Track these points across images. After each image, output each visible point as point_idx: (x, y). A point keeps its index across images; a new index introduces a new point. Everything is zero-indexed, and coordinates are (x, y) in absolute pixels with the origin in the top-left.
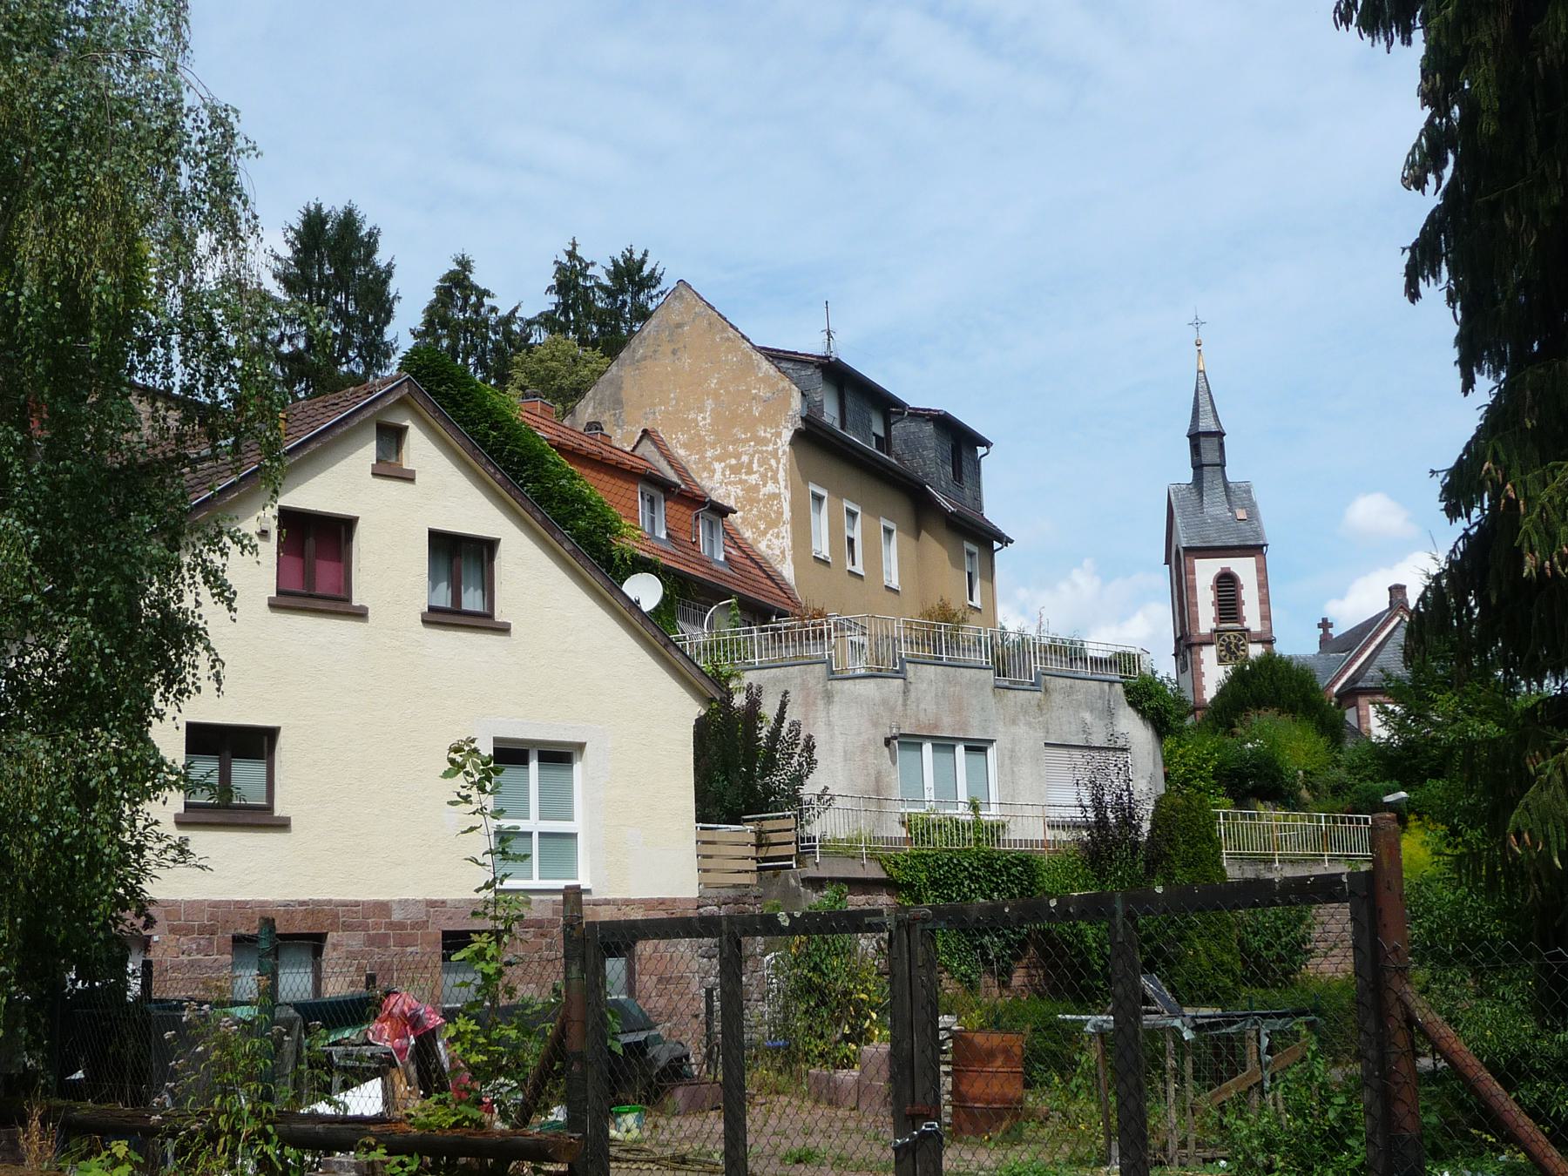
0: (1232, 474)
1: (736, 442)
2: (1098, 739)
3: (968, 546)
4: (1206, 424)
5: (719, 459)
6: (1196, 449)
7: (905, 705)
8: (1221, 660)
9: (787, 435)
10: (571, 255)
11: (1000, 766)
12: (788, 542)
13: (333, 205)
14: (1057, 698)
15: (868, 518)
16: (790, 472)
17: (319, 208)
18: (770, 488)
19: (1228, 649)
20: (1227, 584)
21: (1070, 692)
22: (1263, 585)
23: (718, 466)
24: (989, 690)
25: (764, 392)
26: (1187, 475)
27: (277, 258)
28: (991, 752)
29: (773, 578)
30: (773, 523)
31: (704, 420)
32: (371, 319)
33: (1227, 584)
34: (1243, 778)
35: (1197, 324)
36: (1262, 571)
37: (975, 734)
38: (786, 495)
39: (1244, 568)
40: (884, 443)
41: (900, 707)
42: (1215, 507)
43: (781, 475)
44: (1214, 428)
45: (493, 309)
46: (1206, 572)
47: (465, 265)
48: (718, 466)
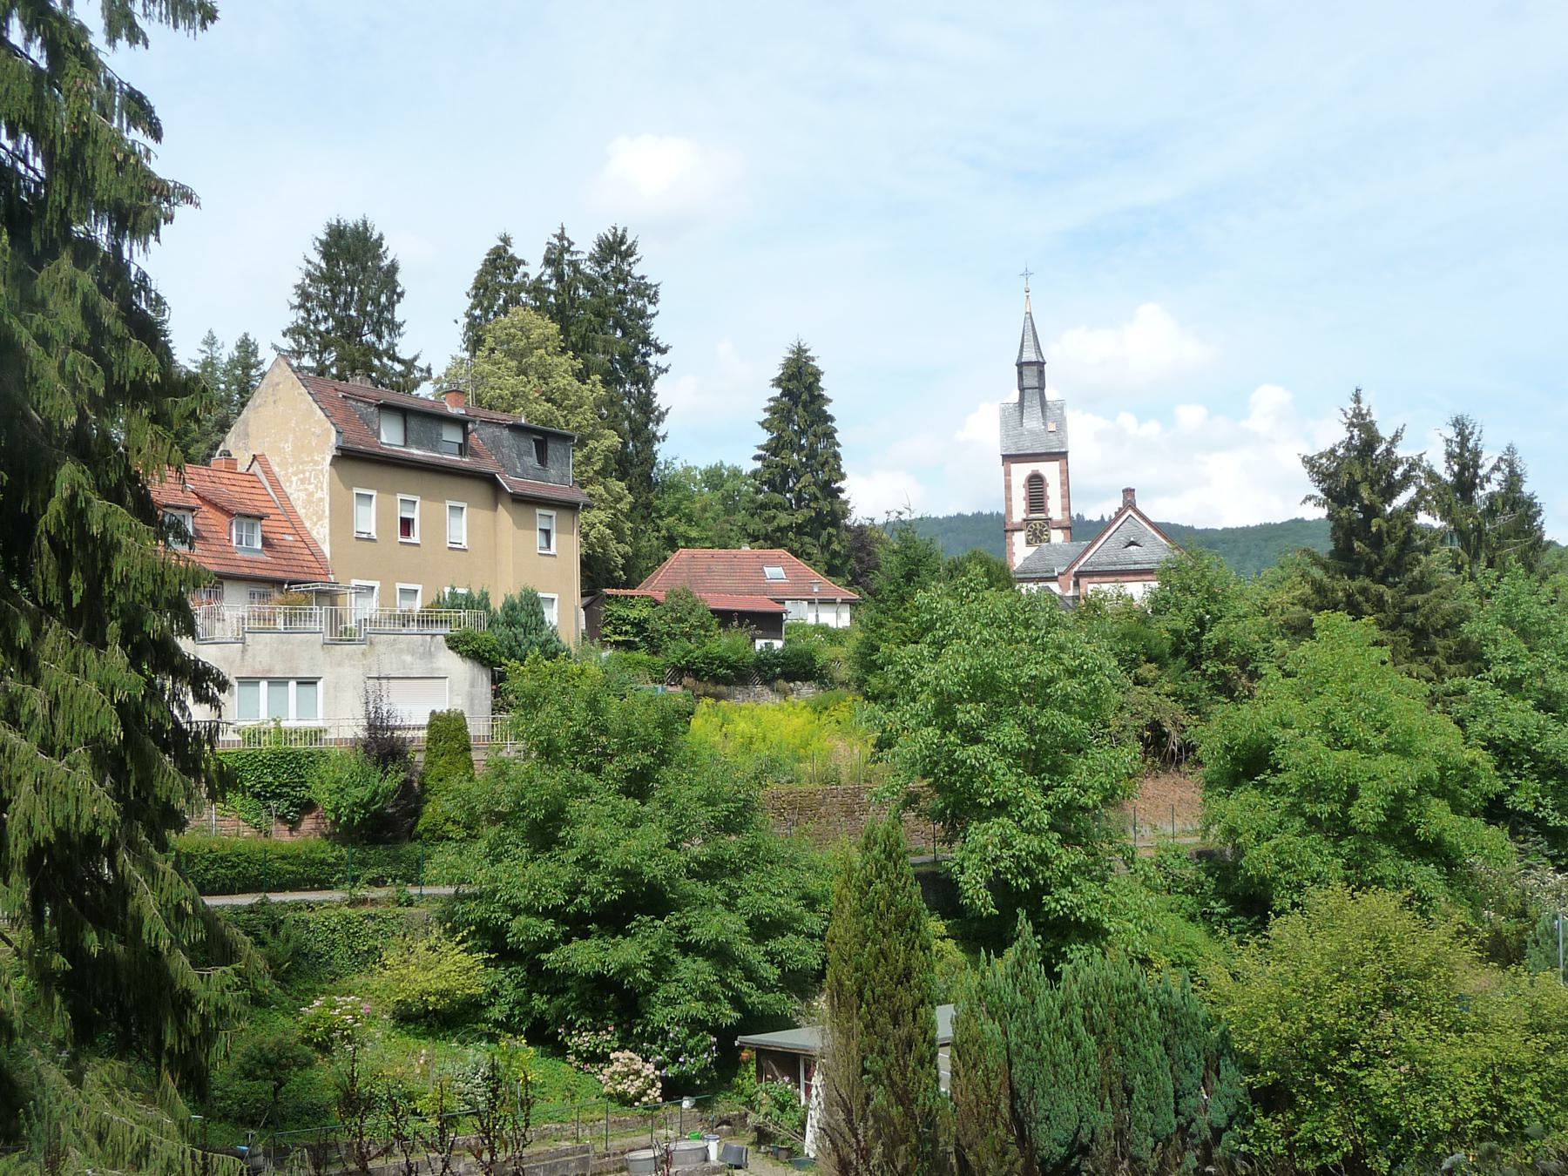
0: (1051, 394)
1: (303, 463)
2: (384, 682)
3: (538, 511)
4: (1029, 355)
5: (295, 474)
6: (1020, 374)
7: (243, 659)
8: (1028, 543)
9: (329, 459)
10: (561, 237)
11: (326, 693)
12: (327, 531)
13: (351, 219)
14: (380, 648)
15: (428, 504)
16: (331, 483)
17: (330, 226)
18: (319, 495)
19: (1034, 534)
20: (1036, 482)
21: (392, 644)
22: (1065, 483)
23: (294, 479)
24: (318, 647)
25: (318, 431)
26: (1014, 396)
27: (309, 262)
28: (320, 684)
29: (316, 554)
30: (320, 518)
31: (288, 447)
32: (383, 299)
33: (1036, 482)
34: (772, 666)
35: (1027, 274)
36: (1065, 472)
37: (305, 674)
38: (327, 499)
39: (1049, 470)
40: (463, 449)
41: (238, 661)
42: (1033, 422)
43: (325, 486)
44: (1034, 358)
45: (526, 275)
46: (1021, 471)
47: (506, 240)
48: (294, 479)
